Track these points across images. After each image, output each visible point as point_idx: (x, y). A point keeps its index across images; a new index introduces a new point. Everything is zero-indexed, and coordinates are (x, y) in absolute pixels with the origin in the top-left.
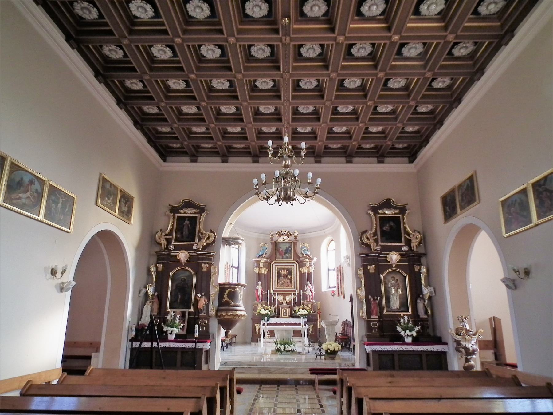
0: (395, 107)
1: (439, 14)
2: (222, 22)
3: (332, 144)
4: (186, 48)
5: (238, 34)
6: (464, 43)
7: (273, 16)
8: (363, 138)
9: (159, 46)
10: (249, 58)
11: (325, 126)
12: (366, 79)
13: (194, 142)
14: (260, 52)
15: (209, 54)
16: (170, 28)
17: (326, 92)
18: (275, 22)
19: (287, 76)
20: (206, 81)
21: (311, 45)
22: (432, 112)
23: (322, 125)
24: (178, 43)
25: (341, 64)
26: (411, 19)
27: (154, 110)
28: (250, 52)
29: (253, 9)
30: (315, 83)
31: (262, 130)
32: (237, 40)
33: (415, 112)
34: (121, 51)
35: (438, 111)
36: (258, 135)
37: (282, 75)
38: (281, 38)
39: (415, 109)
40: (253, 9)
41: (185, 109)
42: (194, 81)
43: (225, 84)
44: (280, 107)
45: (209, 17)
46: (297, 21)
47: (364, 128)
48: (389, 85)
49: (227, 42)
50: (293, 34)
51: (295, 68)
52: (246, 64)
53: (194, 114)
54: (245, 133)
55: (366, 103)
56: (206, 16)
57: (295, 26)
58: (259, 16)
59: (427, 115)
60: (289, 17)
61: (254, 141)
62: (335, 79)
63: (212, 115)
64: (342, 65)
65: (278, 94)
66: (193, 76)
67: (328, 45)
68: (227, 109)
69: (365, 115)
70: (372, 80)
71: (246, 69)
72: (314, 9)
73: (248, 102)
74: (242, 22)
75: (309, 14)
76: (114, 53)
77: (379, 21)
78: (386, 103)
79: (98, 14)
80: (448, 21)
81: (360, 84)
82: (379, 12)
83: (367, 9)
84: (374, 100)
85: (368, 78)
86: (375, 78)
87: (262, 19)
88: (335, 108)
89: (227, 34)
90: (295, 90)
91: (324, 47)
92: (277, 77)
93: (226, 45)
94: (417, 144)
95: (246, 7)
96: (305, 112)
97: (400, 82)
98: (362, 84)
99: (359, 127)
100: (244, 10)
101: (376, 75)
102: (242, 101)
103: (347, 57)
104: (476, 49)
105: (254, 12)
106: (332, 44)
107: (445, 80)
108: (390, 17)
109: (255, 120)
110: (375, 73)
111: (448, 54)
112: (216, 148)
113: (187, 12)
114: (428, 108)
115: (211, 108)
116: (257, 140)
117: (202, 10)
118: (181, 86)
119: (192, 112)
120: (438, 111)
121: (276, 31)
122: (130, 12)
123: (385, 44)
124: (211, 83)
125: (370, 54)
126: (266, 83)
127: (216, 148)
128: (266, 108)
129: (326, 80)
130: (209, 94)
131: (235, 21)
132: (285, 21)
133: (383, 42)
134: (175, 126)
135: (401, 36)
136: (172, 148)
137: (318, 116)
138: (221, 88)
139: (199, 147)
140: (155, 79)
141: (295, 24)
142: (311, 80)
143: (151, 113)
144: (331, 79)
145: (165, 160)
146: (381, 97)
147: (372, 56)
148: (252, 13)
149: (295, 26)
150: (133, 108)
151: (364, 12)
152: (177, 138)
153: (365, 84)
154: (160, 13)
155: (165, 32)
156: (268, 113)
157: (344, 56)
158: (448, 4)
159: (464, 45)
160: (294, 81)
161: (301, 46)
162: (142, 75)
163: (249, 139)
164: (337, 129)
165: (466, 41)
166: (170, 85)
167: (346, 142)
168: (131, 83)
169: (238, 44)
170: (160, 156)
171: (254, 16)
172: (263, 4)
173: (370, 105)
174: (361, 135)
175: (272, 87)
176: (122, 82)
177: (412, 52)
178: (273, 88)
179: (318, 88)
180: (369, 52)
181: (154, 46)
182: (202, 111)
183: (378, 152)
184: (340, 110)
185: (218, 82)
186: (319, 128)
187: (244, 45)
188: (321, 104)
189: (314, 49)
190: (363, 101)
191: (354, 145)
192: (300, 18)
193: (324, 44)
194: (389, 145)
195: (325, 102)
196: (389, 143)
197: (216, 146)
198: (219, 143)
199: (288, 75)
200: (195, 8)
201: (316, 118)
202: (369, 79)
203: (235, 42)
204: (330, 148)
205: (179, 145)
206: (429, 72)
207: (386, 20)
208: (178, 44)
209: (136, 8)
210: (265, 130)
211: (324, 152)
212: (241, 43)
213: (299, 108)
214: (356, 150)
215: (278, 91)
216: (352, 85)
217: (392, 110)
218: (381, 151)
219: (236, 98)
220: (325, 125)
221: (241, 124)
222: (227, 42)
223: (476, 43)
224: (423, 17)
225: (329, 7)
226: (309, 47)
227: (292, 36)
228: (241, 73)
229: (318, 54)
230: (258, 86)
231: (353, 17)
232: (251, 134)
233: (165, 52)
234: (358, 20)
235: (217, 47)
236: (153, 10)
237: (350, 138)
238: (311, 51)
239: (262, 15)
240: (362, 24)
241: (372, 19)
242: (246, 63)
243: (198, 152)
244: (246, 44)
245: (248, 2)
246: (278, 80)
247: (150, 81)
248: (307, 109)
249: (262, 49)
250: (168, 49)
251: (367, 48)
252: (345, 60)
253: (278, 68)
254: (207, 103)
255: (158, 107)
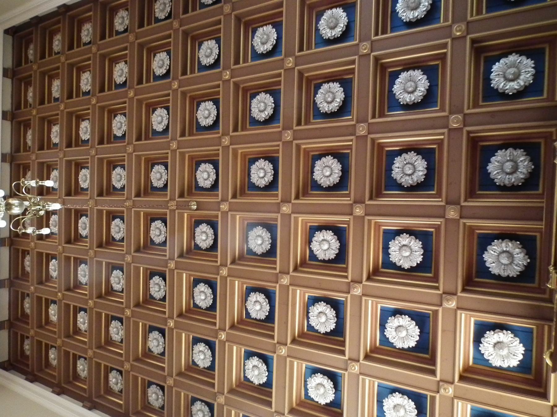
0: (85, 333)
1: (150, 350)
2: (49, 151)
3: (32, 262)
4: (166, 92)
5: (233, 149)
6: (121, 380)
7: (151, 192)
8: (39, 299)
9: (126, 70)
10: (151, 163)
11: (32, 246)
12: (86, 288)
13: (36, 80)
14: (158, 175)
15: (157, 118)
16: (188, 79)
17: (74, 246)
18: (190, 193)
19: (91, 203)
20: (124, 108)
21: (123, 229)
22: (76, 377)
23: (60, 247)
24: (173, 84)
25: (140, 267)
26: (189, 336)
27: (86, 36)
28: (158, 164)
29: (206, 171)
30: (118, 237)
31: (53, 170)
32: (174, 151)
33: (76, 358)
34: (163, 17)
35: (80, 385)
36: (45, 165)
37: (131, 199)
38: (131, 199)
39: (52, 346)
40: (206, 171)
41: (56, 84)
42: (126, 95)
43: (118, 131)
44: (87, 194)
45: (198, 123)
46: (190, 217)
47: (28, 292)
48: (113, 322)
49: (128, 144)
50: (178, 213)
51: (138, 214)
52: (187, 156)
53: (78, 87)
54: (49, 148)
55: (91, 298)
56: (200, 120)
57: (186, 215)
58: (198, 177)
59: (73, 372)
60: (197, 210)
61: (36, 159)
62: (29, 247)
63: (78, 108)
64: (140, 267)
65: (105, 194)
66: (131, 94)
67: (165, 251)
68: (85, 129)
69: (45, 292)
70: (122, 303)
71: (101, 160)
72: (204, 235)
73: (95, 156)
74: (191, 158)
75: (198, 230)
76: (120, 21)
77: (188, 304)
78: (90, 324)
79: (206, 4)
80: (237, 391)
81: (115, 289)
82: (197, 302)
83: (201, 290)
84: (95, 307)
85: (124, 298)
86: (124, 306)
87: (149, 181)
88: (54, 257)
89: (297, 130)
90: (109, 213)
91: (121, 242)
92: (127, 193)
93: (168, 138)
94: (30, 367)
95: (207, 164)
96: (79, 225)
97: (118, 334)
98: (116, 291)
99: (57, 293)
100: (205, 162)
101: (128, 307)
102: (97, 148)
103: (149, 272)
104: (155, 410)
105: (203, 172)
106: (166, 256)
107: (85, 372)
108: (193, 314)
109: (69, 163)
110: (93, 296)
111: (149, 381)
112: (26, 107)
113: (205, 101)
114: (82, 372)
115: (88, 109)
116: (39, 163)
117: (206, 118)
118: (118, 77)
119: (81, 85)
120: (80, 385)
121: (181, 195)
122: (207, 38)
123: (164, 313)
124: (121, 114)
125: (152, 297)
126: (119, 179)
127: (26, 107)
128: (86, 178)
129: (123, 250)
130: (106, 109)
131: (194, 151)
132: (194, 205)
133: (167, 310)
134: (63, 59)
135: (173, 329)
136: (27, 48)
137: (104, 245)
138: (113, 125)
139: (28, 84)
140: (92, 58)
141: (188, 215)
142: (87, 229)
143: (81, 32)
144: (123, 256)
145: (7, 32)
146: (99, 315)
147: (149, 299)
148: (202, 170)
149: (186, 215)
150: (89, 10)
151: (198, 286)
152: (43, 57)
153: (153, 302)
154: (203, 71)
155: (140, 82)
156: (78, 179)
157: (149, 269)
158: (259, 387)
159: (119, 381)
160: (123, 212)
161: (122, 219)
162: (179, 20)
163: (40, 152)
164: (54, 265)
165: (123, 382)
166: (85, 73)
167: (33, 277)
168: (123, 18)
169: (169, 151)
170: (14, 27)
171: (198, 172)
172: (210, 183)
173: (89, 304)
174: (44, 296)
175: (114, 186)
176: (126, 6)
177: (153, 343)
178: (112, 188)
179: (79, 237)
180: (154, 296)
181: (126, 65)
182: (53, 104)
183: (17, 319)
184: (52, 262)
185: (121, 123)
186: (56, 242)
187: (167, 158)
188: (90, 244)
189: (119, 232)
190: (35, 280)
191: (29, 288)
192: (193, 220)
193: (166, 246)
194: (29, 333)
195: (93, 250)
196: (32, 333)
197: (29, 107)
198: (34, 112)
199: (174, 208)
200: (208, 110)
201: (139, 247)
202: (122, 299)
203: (172, 148)
204: (24, 257)
205: (31, 57)
206: (130, 365)
207: (188, 310)
208: (127, 93)
209: (162, 58)
210: (54, 175)
211: (18, 250)
212: (169, 155)
213: (84, 218)
214: (20, 290)
215: (109, 194)
216: (115, 280)
217: (80, 329)
218: (18, 323)
219: (101, 142)
220: (61, 250)
221: (64, 144)
222: (128, 144)
223: (121, 391)
224: (147, 335)
225: (260, 255)
226: (162, 230)
227: (177, 211)
228: (134, 152)
229: (154, 239)
230: (116, 170)
231: (245, 283)
232: (47, 156)
233: (160, 67)
234: (190, 283)
235: (165, 128)
236: (207, 65)
237: (40, 283)
238: (157, 233)
239: (198, 180)
240: (143, 277)
241: (191, 295)
242: (145, 158)
243: (20, 80)
244: (169, 161)
245: (213, 167)
246: (124, 194)
247: (126, 40)
248: (84, 228)
249: (161, 177)
250: (165, 72)
251: (160, 293)
252: (146, 270)
253: (138, 195)
254: (95, 105)
255: (90, 43)
